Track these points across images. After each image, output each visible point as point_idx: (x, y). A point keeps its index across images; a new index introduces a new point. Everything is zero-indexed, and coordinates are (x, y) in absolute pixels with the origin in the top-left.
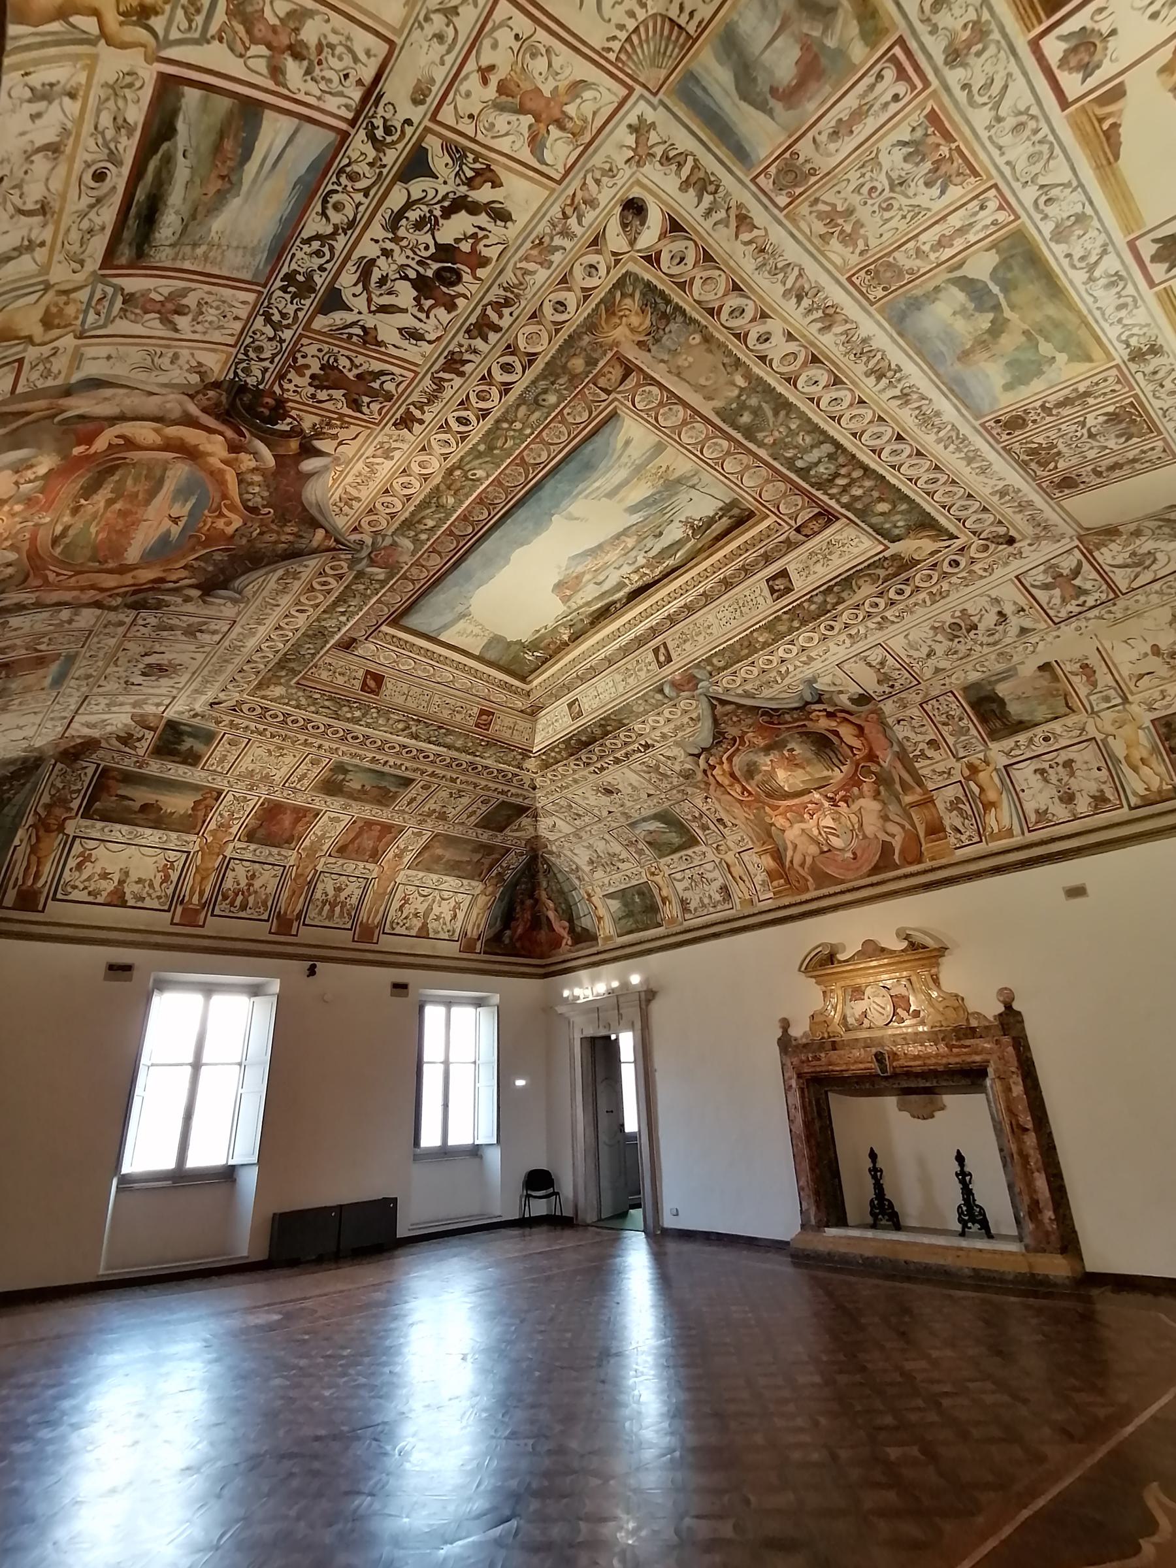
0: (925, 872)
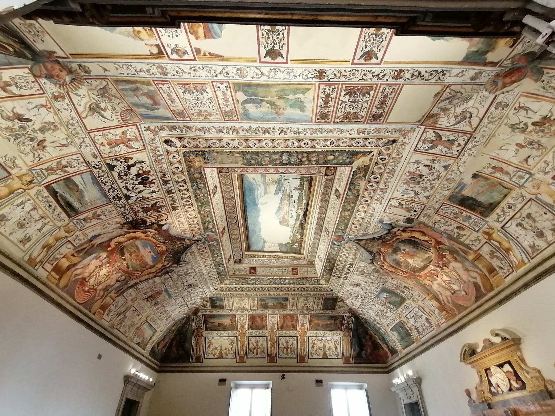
0: (497, 295)
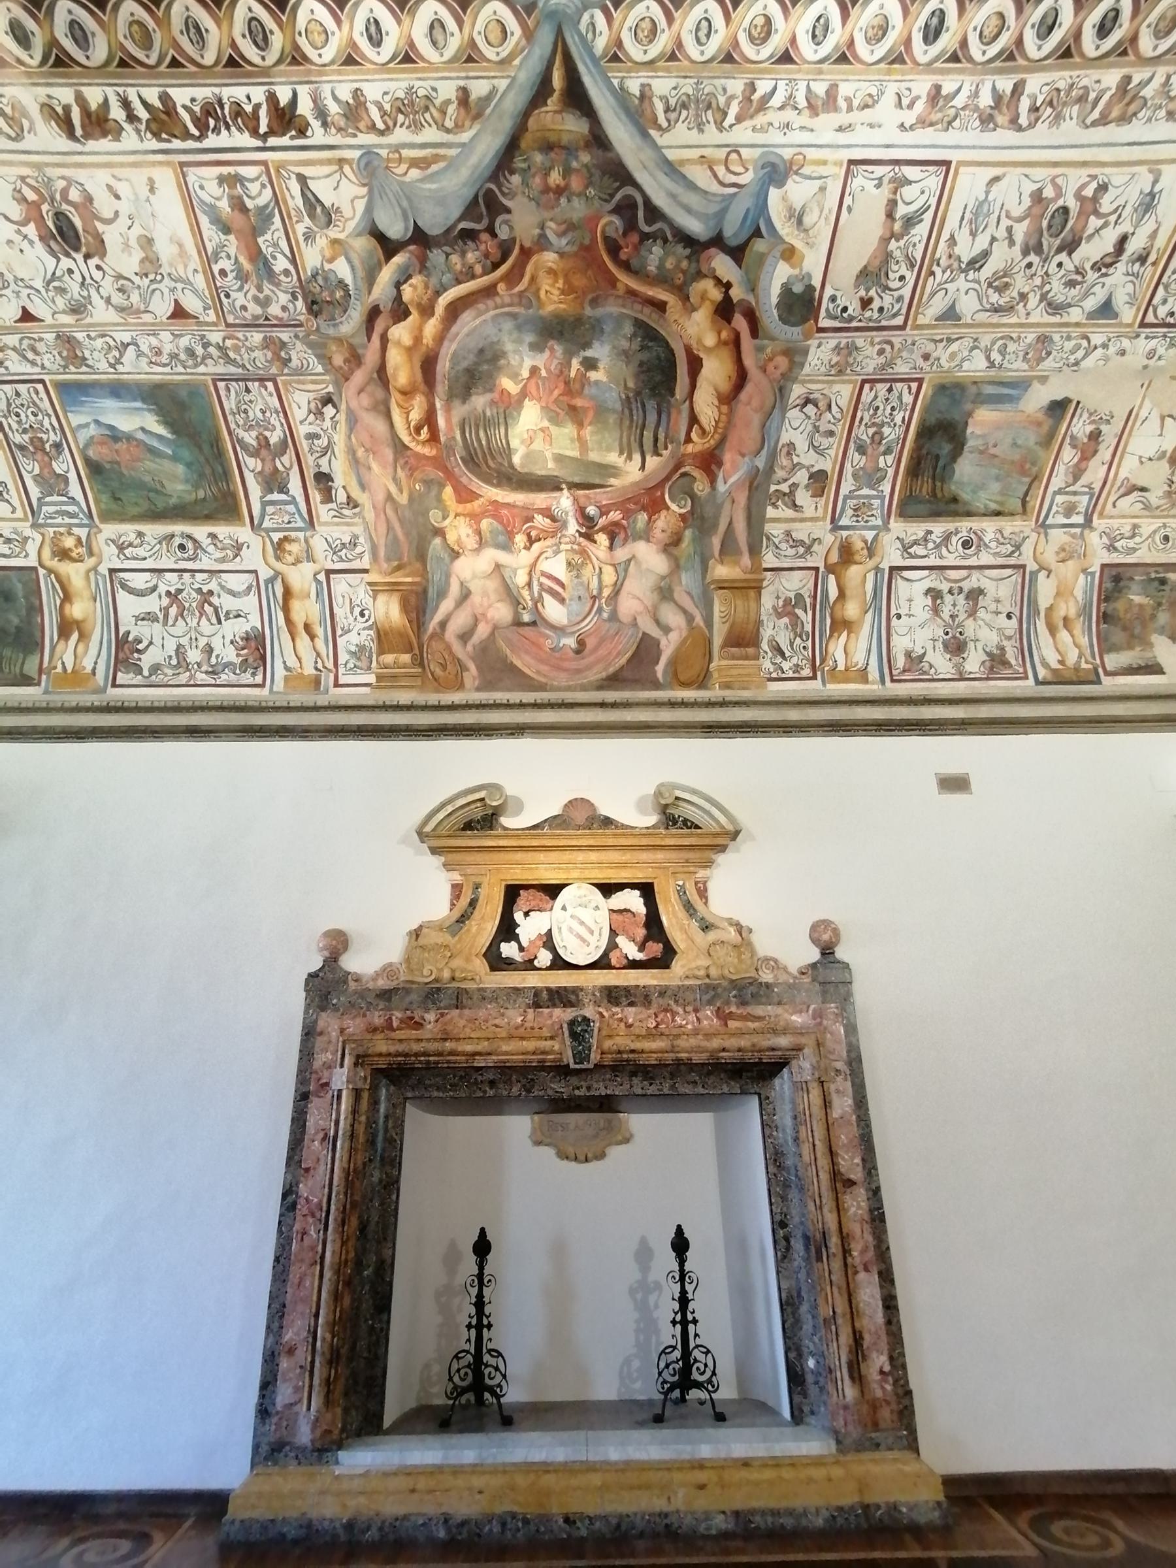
0: (710, 704)
